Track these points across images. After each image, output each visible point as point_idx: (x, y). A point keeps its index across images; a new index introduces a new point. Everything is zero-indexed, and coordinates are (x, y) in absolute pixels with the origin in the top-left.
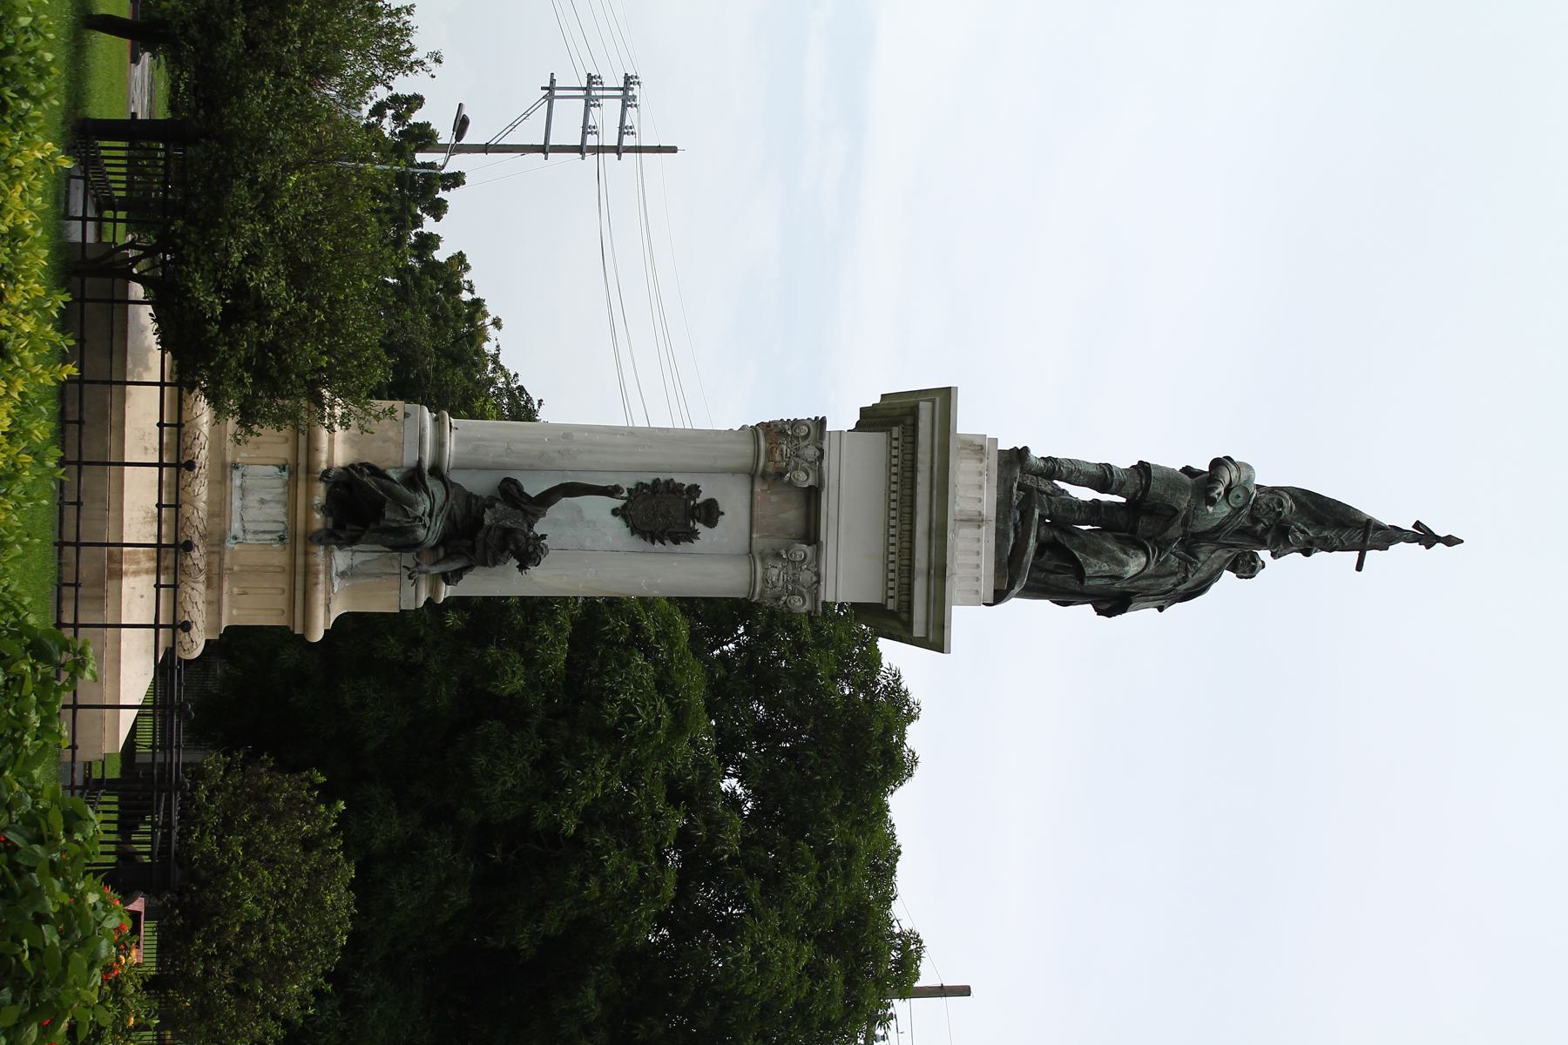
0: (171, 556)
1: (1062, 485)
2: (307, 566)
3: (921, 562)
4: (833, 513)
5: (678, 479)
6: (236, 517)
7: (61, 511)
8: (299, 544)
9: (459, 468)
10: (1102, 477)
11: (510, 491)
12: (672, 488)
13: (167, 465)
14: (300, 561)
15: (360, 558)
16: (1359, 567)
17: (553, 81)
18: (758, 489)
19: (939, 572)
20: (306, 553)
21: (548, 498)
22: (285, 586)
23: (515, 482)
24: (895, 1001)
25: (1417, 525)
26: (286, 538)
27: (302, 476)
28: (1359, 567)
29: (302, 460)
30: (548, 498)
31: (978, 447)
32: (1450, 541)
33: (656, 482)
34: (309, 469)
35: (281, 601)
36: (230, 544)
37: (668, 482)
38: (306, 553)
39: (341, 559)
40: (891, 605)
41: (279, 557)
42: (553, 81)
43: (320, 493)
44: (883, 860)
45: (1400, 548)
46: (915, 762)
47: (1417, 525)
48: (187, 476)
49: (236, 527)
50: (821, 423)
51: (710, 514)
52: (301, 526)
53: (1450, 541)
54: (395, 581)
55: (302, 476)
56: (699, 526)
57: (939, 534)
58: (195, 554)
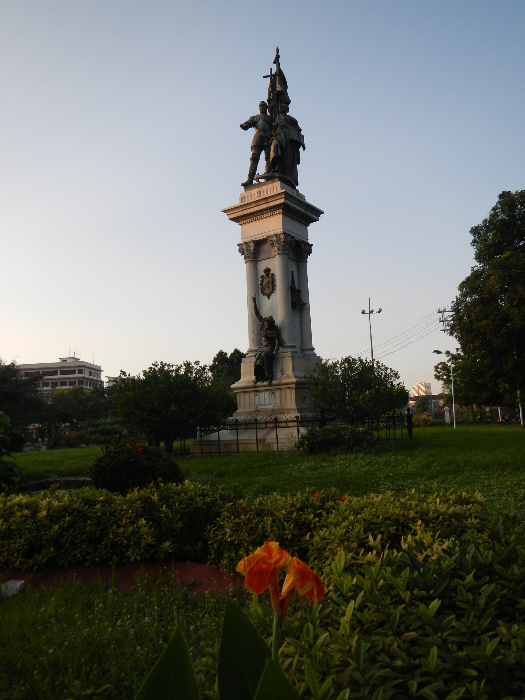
2: (277, 385)
3: (303, 211)
4: (260, 236)
5: (260, 282)
6: (269, 407)
8: (272, 389)
10: (255, 160)
14: (277, 387)
15: (279, 370)
17: (442, 330)
18: (260, 259)
19: (288, 200)
20: (274, 385)
22: (263, 393)
25: (274, 63)
26: (273, 391)
27: (256, 389)
29: (253, 389)
31: (242, 199)
32: (278, 50)
33: (261, 288)
34: (255, 387)
35: (288, 391)
36: (275, 408)
38: (274, 385)
39: (279, 375)
40: (281, 211)
41: (277, 393)
42: (442, 330)
43: (259, 384)
44: (298, 160)
45: (281, 67)
47: (274, 63)
48: (259, 420)
49: (272, 406)
50: (238, 245)
51: (267, 271)
52: (269, 388)
53: (278, 50)
55: (256, 389)
56: (271, 273)
57: (266, 199)
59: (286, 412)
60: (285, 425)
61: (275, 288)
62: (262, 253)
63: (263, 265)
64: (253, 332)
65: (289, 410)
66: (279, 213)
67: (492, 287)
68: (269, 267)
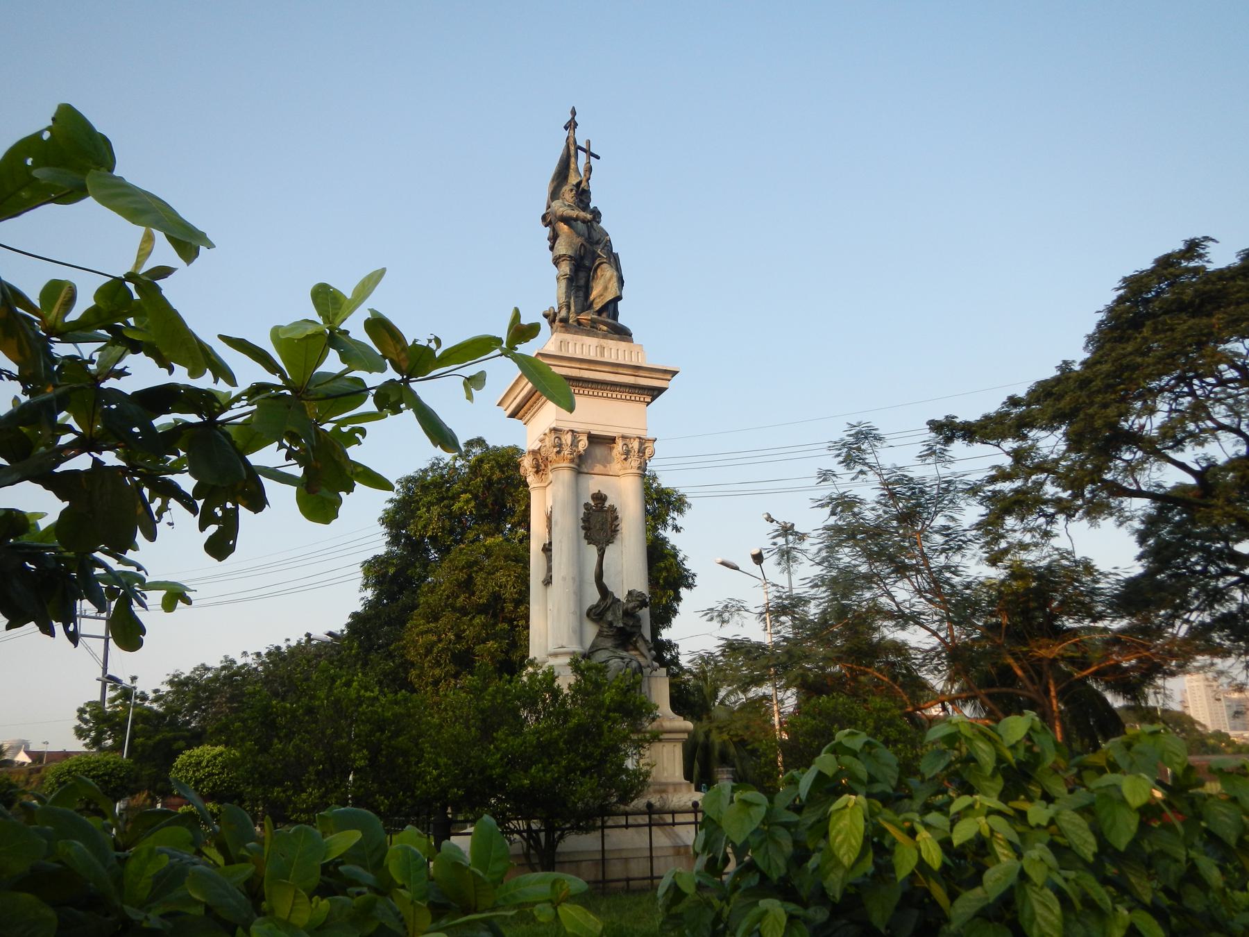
0: (655, 817)
1: (169, 477)
4: (600, 428)
7: (634, 891)
9: (581, 642)
11: (596, 614)
12: (586, 519)
13: (603, 822)
16: (598, 158)
21: (603, 590)
23: (590, 610)
24: (1088, 355)
25: (566, 128)
28: (598, 158)
30: (603, 590)
32: (574, 113)
33: (584, 528)
37: (584, 521)
46: (1125, 280)
47: (566, 128)
51: (600, 498)
53: (574, 113)
54: (653, 681)
56: (607, 504)
58: (653, 801)
59: (671, 789)
60: (669, 818)
63: (594, 484)
64: (574, 613)
65: (676, 786)
67: (500, 587)
68: (603, 492)
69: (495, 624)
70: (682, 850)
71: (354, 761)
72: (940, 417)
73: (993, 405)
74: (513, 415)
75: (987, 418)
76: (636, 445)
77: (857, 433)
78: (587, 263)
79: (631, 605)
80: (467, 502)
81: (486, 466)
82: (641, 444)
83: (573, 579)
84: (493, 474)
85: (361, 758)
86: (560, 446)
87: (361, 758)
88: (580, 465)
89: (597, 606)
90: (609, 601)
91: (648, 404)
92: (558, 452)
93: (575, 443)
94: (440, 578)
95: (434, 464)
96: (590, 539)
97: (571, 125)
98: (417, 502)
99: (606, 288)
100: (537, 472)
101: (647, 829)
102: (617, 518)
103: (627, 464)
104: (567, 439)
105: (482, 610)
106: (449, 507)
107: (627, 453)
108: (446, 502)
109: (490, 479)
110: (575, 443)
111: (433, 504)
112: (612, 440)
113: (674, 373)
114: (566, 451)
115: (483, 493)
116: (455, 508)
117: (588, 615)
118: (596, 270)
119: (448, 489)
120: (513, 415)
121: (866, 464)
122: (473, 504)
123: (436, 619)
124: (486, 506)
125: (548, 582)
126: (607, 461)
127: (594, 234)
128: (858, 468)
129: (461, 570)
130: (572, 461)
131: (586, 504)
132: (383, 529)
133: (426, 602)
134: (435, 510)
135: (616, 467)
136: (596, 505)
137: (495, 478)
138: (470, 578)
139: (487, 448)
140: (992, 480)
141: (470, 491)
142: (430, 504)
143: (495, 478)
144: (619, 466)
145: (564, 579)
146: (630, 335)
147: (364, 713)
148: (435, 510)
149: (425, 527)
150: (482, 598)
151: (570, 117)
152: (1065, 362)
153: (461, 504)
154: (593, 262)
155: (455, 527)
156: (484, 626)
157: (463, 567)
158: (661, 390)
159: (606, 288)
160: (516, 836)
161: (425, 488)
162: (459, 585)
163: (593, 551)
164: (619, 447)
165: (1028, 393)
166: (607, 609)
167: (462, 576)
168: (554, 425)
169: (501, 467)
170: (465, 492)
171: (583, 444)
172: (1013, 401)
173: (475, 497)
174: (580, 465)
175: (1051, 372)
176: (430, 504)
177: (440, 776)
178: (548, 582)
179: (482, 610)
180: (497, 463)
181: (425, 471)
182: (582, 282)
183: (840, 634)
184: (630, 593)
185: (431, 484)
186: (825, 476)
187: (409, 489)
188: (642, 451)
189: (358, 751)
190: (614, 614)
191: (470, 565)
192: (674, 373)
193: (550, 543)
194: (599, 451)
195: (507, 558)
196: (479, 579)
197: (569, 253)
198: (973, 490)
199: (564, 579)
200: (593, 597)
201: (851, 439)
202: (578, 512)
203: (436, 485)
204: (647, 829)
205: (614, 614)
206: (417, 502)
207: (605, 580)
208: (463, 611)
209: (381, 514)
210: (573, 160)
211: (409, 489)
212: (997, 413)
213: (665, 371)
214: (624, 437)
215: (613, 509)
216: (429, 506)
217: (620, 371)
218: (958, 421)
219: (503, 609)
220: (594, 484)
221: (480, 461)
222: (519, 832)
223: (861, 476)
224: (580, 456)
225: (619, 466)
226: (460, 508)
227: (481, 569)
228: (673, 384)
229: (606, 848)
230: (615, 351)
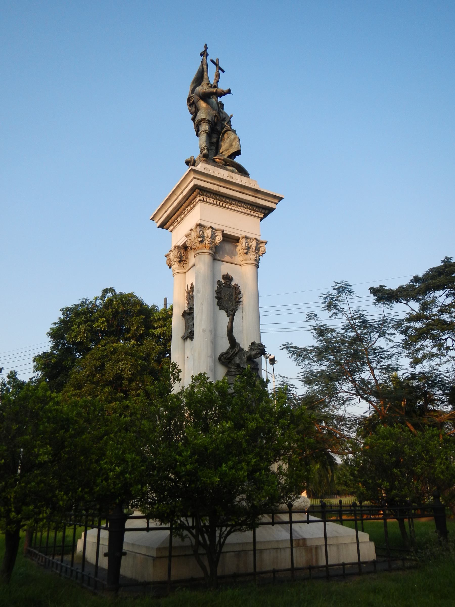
4: (230, 230)
23: (222, 355)
25: (201, 55)
32: (206, 47)
33: (217, 298)
51: (228, 278)
53: (206, 47)
56: (233, 283)
61: (240, 306)
62: (221, 253)
63: (225, 269)
66: (258, 217)
67: (121, 370)
68: (231, 274)
69: (116, 394)
70: (301, 543)
71: (37, 456)
72: (376, 286)
73: (405, 281)
74: (162, 226)
75: (401, 287)
76: (254, 244)
77: (339, 288)
78: (219, 128)
79: (254, 353)
80: (102, 323)
81: (115, 303)
82: (257, 244)
83: (210, 331)
84: (119, 307)
85: (45, 453)
86: (203, 237)
87: (45, 453)
88: (216, 253)
89: (227, 353)
90: (237, 349)
91: (261, 219)
92: (201, 242)
93: (213, 237)
94: (82, 368)
95: (83, 302)
96: (221, 305)
97: (204, 54)
98: (72, 322)
99: (231, 145)
100: (180, 262)
101: (294, 525)
102: (240, 293)
103: (247, 257)
104: (208, 233)
105: (109, 383)
106: (90, 326)
107: (248, 248)
108: (89, 323)
109: (117, 311)
110: (213, 237)
111: (82, 324)
112: (236, 240)
113: (280, 199)
114: (207, 242)
115: (112, 319)
116: (94, 326)
117: (220, 359)
118: (223, 135)
119: (91, 316)
120: (162, 226)
121: (337, 309)
122: (106, 324)
123: (80, 388)
124: (113, 327)
125: (189, 335)
126: (233, 254)
127: (221, 115)
128: (333, 311)
129: (98, 360)
130: (211, 249)
131: (219, 281)
132: (50, 339)
133: (75, 377)
134: (83, 327)
135: (238, 259)
136: (225, 283)
137: (120, 309)
138: (103, 365)
139: (115, 294)
140: (409, 320)
141: (105, 317)
142: (80, 323)
143: (120, 309)
144: (241, 258)
145: (204, 331)
146: (248, 175)
147: (50, 411)
148: (83, 327)
149: (76, 336)
150: (109, 376)
151: (204, 49)
152: (446, 258)
153: (99, 324)
154: (222, 129)
155: (94, 335)
156: (110, 393)
157: (100, 358)
158: (271, 210)
159: (231, 145)
160: (185, 532)
161: (77, 314)
162: (96, 369)
163: (223, 314)
164: (243, 244)
165: (424, 276)
166: (235, 355)
167: (98, 363)
168: (199, 222)
169: (124, 304)
170: (101, 317)
171: (219, 238)
172: (416, 279)
173: (107, 321)
174: (216, 253)
175: (438, 263)
176: (80, 323)
177: (122, 473)
178: (189, 335)
179: (109, 383)
180: (122, 301)
181: (78, 306)
182: (214, 140)
183: (152, 455)
184: (253, 344)
185: (81, 312)
186: (311, 316)
187: (68, 315)
188: (257, 249)
189: (41, 446)
190: (241, 358)
191: (103, 357)
192: (280, 199)
193: (191, 309)
194: (228, 247)
195: (126, 353)
196: (108, 366)
197: (208, 118)
198: (398, 325)
199: (204, 331)
200: (225, 345)
201: (335, 292)
202: (213, 287)
203: (83, 313)
204: (294, 525)
205: (241, 358)
206: (72, 322)
207: (235, 334)
208: (97, 383)
209: (48, 330)
210: (205, 73)
211: (68, 315)
212: (407, 285)
213: (275, 197)
214: (246, 238)
215: (236, 288)
216: (79, 324)
217: (246, 191)
218: (386, 288)
219: (122, 383)
220: (225, 269)
221: (111, 300)
222: (188, 528)
223: (335, 316)
224: (216, 247)
225: (241, 258)
226: (98, 326)
227: (110, 360)
228: (279, 207)
229: (257, 540)
230: (238, 179)
